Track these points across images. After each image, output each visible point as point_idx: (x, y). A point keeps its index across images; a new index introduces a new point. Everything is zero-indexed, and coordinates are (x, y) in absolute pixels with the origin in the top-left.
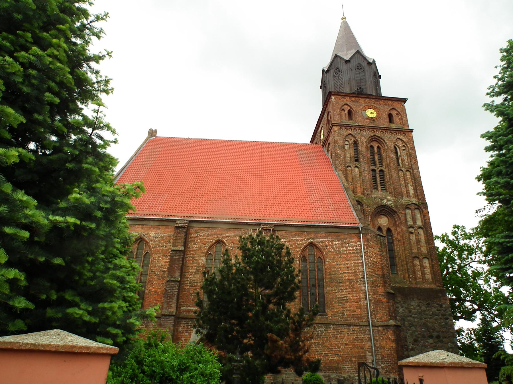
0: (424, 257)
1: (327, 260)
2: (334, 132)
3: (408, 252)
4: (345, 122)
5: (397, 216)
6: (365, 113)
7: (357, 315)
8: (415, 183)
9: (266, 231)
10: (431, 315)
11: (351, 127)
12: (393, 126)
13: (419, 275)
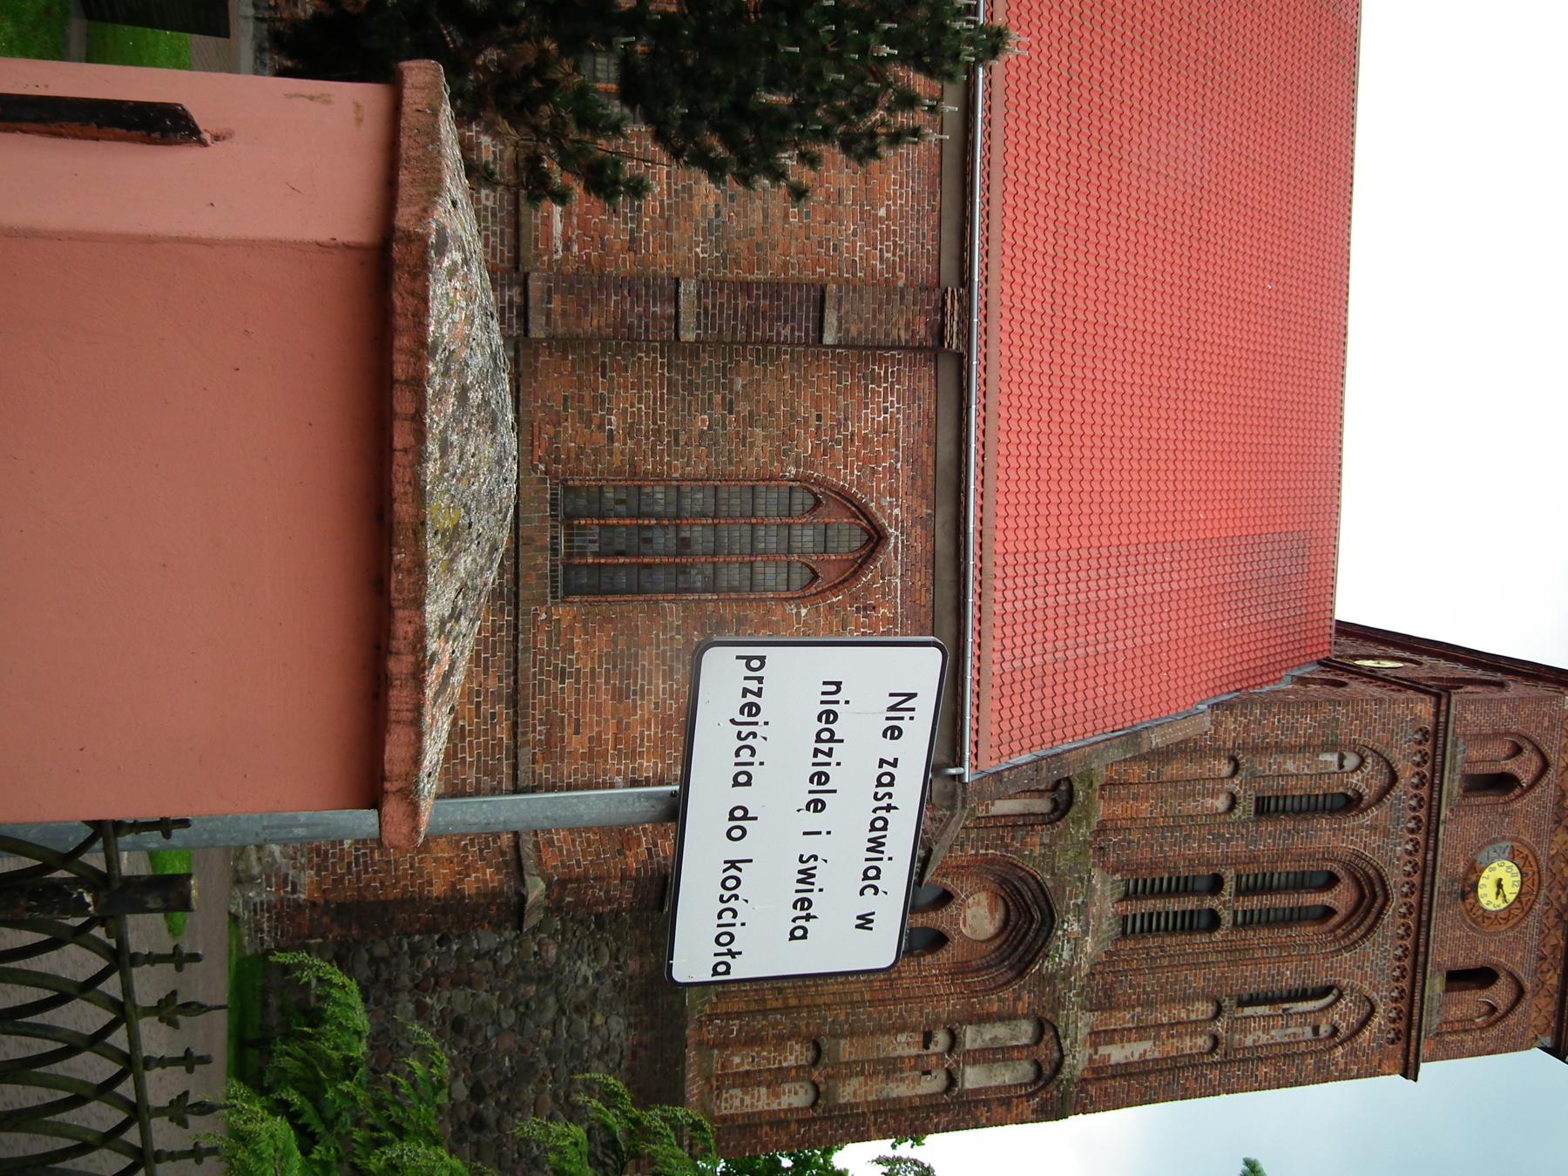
0: (822, 1088)
1: (804, 612)
2: (1407, 701)
3: (842, 1017)
4: (1454, 757)
5: (1001, 980)
6: (1499, 857)
7: (562, 739)
8: (1161, 1071)
9: (935, 310)
10: (567, 1097)
11: (1431, 781)
12: (1436, 985)
13: (739, 1061)
